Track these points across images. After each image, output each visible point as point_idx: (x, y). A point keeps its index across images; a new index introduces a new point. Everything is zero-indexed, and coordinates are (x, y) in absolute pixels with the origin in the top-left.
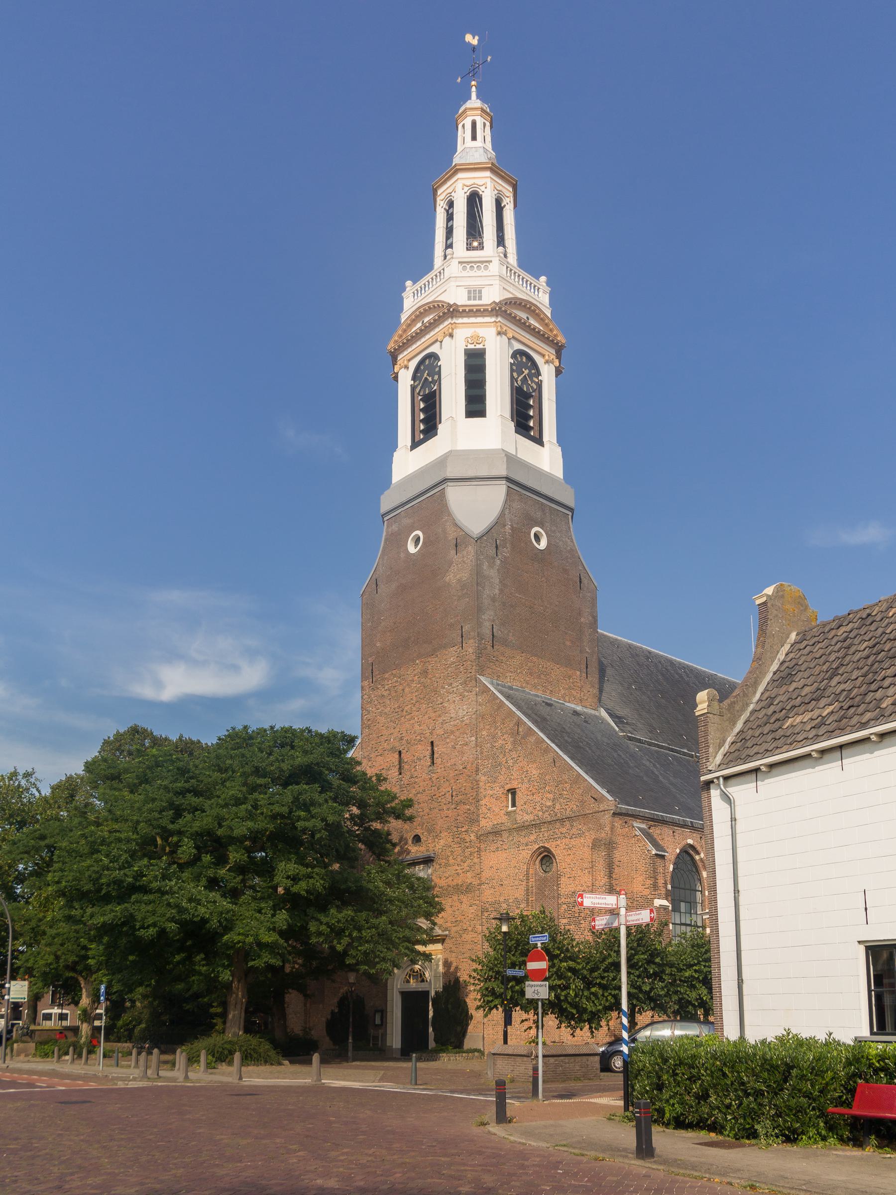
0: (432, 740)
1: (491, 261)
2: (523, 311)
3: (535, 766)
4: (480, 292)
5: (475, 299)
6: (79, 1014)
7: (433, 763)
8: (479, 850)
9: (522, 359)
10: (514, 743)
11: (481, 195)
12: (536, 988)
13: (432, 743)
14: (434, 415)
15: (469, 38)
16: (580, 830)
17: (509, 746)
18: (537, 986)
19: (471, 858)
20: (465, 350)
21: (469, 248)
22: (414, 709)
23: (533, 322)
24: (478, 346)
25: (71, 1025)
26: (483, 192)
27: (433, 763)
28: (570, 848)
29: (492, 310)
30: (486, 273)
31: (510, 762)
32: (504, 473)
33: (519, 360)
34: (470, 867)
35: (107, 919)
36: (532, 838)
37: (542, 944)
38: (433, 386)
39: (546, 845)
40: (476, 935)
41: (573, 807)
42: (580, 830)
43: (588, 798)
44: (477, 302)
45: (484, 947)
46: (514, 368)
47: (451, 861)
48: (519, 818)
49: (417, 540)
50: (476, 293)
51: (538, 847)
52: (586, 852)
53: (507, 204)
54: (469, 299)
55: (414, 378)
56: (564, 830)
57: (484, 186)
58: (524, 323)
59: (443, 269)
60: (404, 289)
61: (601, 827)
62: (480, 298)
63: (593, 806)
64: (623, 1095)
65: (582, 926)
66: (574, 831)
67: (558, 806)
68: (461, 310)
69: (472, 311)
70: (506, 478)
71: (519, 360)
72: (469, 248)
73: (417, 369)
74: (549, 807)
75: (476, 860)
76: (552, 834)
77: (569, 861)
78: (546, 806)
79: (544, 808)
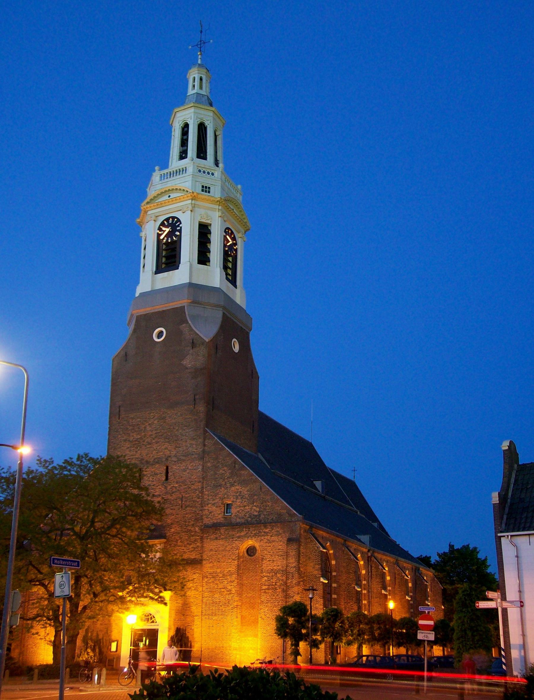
7: (167, 479)
8: (202, 539)
11: (207, 126)
12: (426, 634)
17: (228, 474)
18: (428, 633)
20: (199, 222)
21: (199, 157)
27: (167, 479)
32: (222, 303)
37: (72, 592)
45: (203, 601)
47: (179, 544)
49: (160, 335)
60: (154, 171)
62: (209, 192)
65: (277, 591)
67: (262, 516)
74: (256, 516)
76: (258, 532)
78: (254, 515)
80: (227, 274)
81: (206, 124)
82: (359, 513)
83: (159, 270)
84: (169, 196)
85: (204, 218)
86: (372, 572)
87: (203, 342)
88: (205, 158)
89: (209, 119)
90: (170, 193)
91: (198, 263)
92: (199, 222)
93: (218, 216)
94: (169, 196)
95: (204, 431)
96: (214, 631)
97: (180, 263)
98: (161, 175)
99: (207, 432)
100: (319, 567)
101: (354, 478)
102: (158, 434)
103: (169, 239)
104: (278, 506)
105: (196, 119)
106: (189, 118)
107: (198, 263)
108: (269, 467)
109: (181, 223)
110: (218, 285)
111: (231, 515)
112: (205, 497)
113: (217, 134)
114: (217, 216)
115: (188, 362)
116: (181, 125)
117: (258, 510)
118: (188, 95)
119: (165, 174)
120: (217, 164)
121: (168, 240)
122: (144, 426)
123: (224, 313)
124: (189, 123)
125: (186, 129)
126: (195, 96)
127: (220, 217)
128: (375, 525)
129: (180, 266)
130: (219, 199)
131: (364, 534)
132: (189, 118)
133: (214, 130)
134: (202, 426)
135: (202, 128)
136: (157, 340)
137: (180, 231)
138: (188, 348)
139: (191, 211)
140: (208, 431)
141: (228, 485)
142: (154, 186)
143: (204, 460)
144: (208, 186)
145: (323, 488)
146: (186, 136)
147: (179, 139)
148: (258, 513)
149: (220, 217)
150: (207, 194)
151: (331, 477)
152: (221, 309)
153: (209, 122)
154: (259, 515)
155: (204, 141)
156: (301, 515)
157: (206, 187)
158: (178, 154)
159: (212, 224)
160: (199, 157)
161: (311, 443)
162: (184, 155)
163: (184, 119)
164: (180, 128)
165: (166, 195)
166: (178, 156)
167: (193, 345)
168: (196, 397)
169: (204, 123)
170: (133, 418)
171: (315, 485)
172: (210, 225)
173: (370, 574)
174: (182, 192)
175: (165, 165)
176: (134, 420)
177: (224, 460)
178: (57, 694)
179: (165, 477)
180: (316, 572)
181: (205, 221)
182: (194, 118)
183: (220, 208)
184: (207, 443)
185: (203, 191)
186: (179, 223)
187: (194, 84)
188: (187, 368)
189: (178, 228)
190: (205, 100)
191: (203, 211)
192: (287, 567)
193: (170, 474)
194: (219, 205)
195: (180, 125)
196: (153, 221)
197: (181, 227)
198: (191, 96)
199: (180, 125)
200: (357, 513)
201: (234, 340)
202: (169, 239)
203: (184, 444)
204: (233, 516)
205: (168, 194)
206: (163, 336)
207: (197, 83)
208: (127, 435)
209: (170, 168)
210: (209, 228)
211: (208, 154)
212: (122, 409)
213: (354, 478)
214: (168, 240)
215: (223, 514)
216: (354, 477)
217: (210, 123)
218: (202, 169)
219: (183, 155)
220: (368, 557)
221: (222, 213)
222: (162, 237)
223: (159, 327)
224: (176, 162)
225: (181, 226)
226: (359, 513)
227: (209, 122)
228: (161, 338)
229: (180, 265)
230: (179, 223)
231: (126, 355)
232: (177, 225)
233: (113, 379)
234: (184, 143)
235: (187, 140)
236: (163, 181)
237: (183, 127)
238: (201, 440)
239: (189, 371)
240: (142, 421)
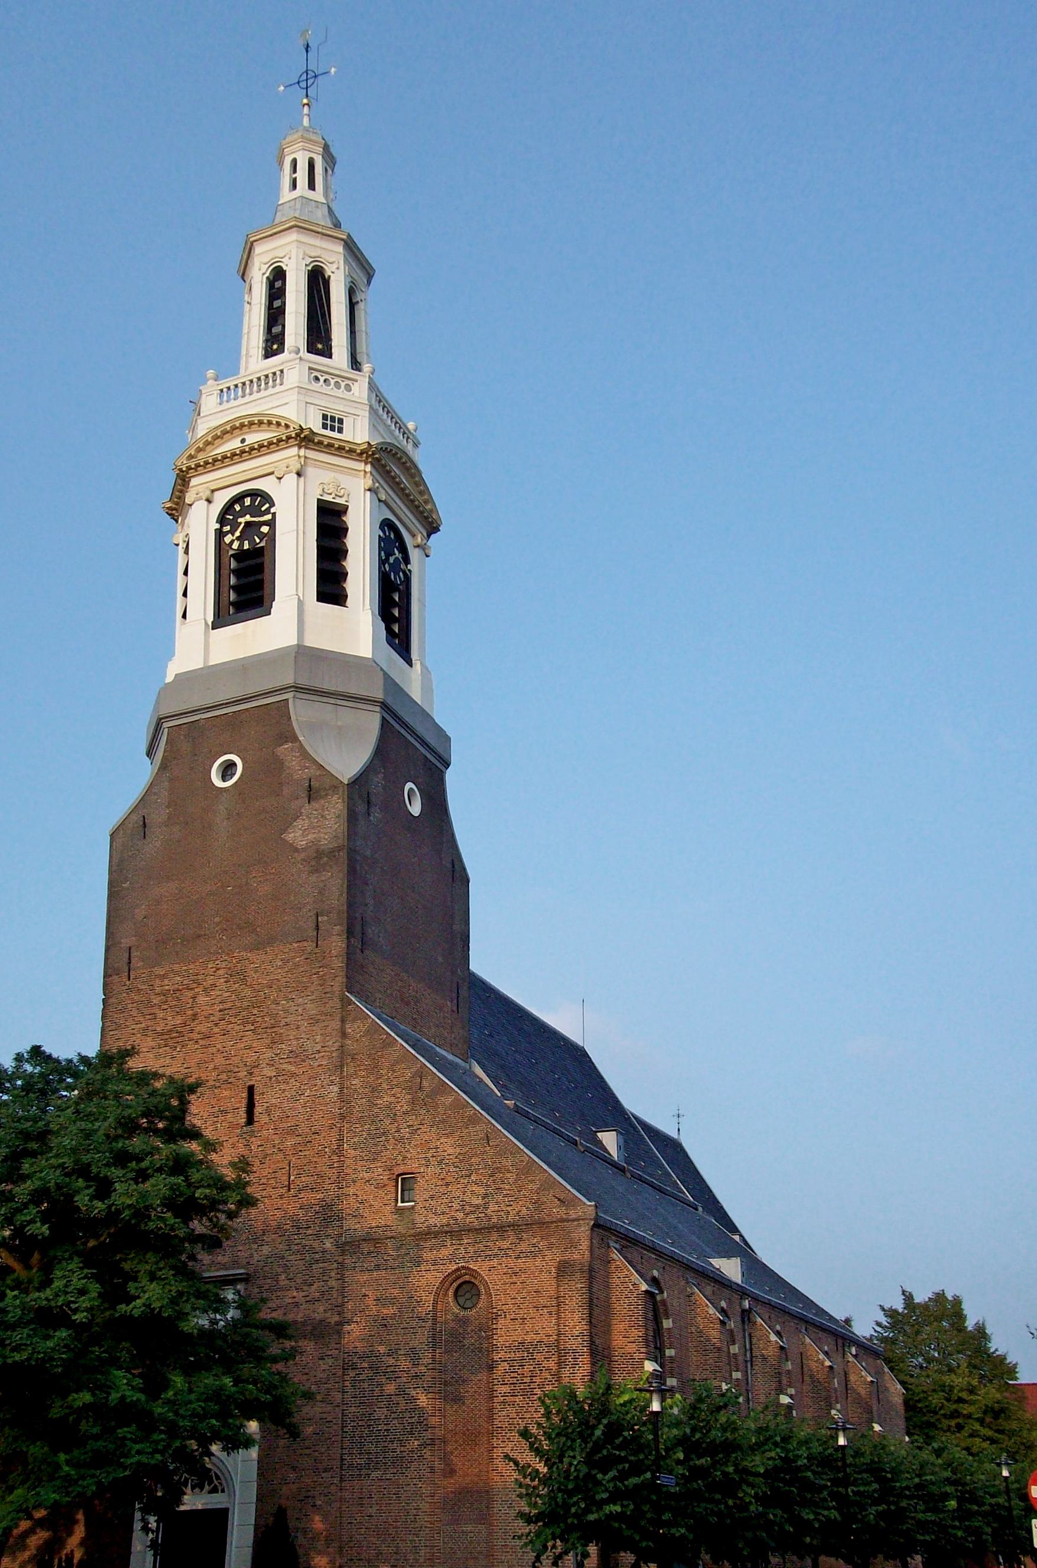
0: (251, 1083)
1: (357, 381)
3: (450, 1141)
4: (341, 421)
5: (333, 429)
7: (250, 1120)
10: (413, 1102)
11: (329, 277)
13: (251, 1090)
14: (260, 585)
15: (192, 1359)
16: (534, 1246)
19: (325, 1278)
21: (312, 349)
22: (216, 1030)
23: (253, 438)
24: (338, 500)
26: (333, 272)
27: (250, 1120)
28: (516, 1274)
29: (361, 454)
30: (347, 395)
31: (405, 1132)
32: (379, 695)
33: (387, 534)
34: (323, 1293)
36: (445, 1252)
38: (258, 540)
39: (471, 1266)
40: (329, 1408)
41: (519, 1210)
42: (534, 1246)
43: (548, 1198)
44: (335, 435)
45: (345, 1430)
48: (420, 1219)
49: (228, 769)
50: (332, 422)
51: (455, 1267)
52: (547, 1282)
53: (361, 300)
54: (325, 426)
55: (222, 520)
56: (505, 1244)
57: (287, 258)
59: (282, 371)
60: (205, 381)
61: (573, 1245)
62: (340, 431)
63: (558, 1211)
66: (523, 1246)
67: (493, 1207)
68: (316, 441)
69: (343, 448)
70: (382, 703)
71: (387, 534)
73: (228, 508)
74: (477, 1206)
75: (333, 1283)
77: (513, 1294)
78: (471, 1205)
79: (467, 1207)
80: (389, 630)
81: (328, 273)
82: (700, 1209)
83: (220, 620)
84: (243, 441)
85: (329, 492)
86: (751, 1349)
87: (335, 785)
88: (327, 353)
89: (334, 260)
91: (318, 600)
92: (319, 500)
93: (365, 490)
94: (243, 441)
95: (342, 1000)
96: (373, 1511)
97: (274, 600)
98: (222, 391)
99: (350, 1002)
100: (640, 1334)
101: (679, 1134)
102: (226, 1012)
103: (246, 542)
104: (532, 1181)
105: (303, 259)
106: (285, 256)
107: (318, 600)
108: (499, 1095)
109: (272, 504)
110: (368, 654)
111: (413, 1207)
112: (348, 1162)
113: (354, 301)
114: (363, 490)
115: (298, 835)
117: (482, 1191)
118: (280, 203)
119: (232, 387)
120: (355, 364)
121: (241, 545)
122: (190, 994)
123: (383, 718)
125: (278, 284)
126: (298, 206)
127: (369, 490)
128: (737, 1238)
129: (273, 605)
130: (365, 446)
131: (729, 1257)
132: (285, 256)
133: (348, 286)
134: (337, 989)
135: (317, 280)
136: (218, 783)
137: (271, 524)
138: (298, 802)
139: (299, 474)
140: (353, 999)
141: (405, 1132)
142: (203, 417)
143: (342, 1072)
145: (619, 1148)
146: (280, 301)
147: (262, 328)
148: (484, 1198)
149: (369, 490)
150: (335, 435)
151: (635, 1128)
152: (378, 709)
153: (335, 266)
154: (486, 1206)
155: (323, 315)
156: (590, 1202)
157: (333, 419)
158: (261, 344)
159: (350, 508)
160: (312, 349)
161: (583, 1047)
162: (275, 347)
163: (272, 259)
164: (265, 280)
165: (238, 436)
166: (260, 349)
167: (312, 793)
168: (320, 919)
169: (322, 267)
170: (163, 977)
171: (601, 1142)
173: (748, 1355)
174: (264, 427)
175: (229, 363)
176: (166, 982)
177: (394, 1071)
179: (245, 1115)
180: (632, 1348)
181: (334, 498)
182: (297, 255)
183: (369, 468)
184: (350, 1031)
186: (267, 505)
187: (294, 176)
188: (296, 850)
190: (323, 215)
192: (558, 1335)
193: (258, 1109)
194: (366, 464)
195: (263, 274)
196: (206, 503)
197: (274, 514)
198: (287, 204)
199: (263, 274)
200: (697, 1209)
201: (409, 785)
202: (246, 542)
203: (293, 1034)
204: (417, 1208)
205: (242, 434)
206: (235, 774)
207: (302, 176)
208: (148, 1017)
209: (242, 372)
211: (334, 343)
212: (134, 954)
213: (679, 1134)
214: (241, 545)
215: (393, 1204)
216: (679, 1130)
217: (338, 268)
218: (322, 376)
219: (274, 343)
220: (743, 1311)
221: (374, 480)
222: (228, 539)
223: (225, 754)
224: (257, 362)
225: (273, 510)
226: (700, 1209)
227: (335, 266)
228: (231, 778)
229: (274, 603)
230: (267, 505)
231: (144, 823)
232: (263, 509)
233: (111, 884)
234: (275, 316)
235: (281, 311)
236: (225, 406)
238: (336, 1024)
239: (303, 855)
240: (185, 982)
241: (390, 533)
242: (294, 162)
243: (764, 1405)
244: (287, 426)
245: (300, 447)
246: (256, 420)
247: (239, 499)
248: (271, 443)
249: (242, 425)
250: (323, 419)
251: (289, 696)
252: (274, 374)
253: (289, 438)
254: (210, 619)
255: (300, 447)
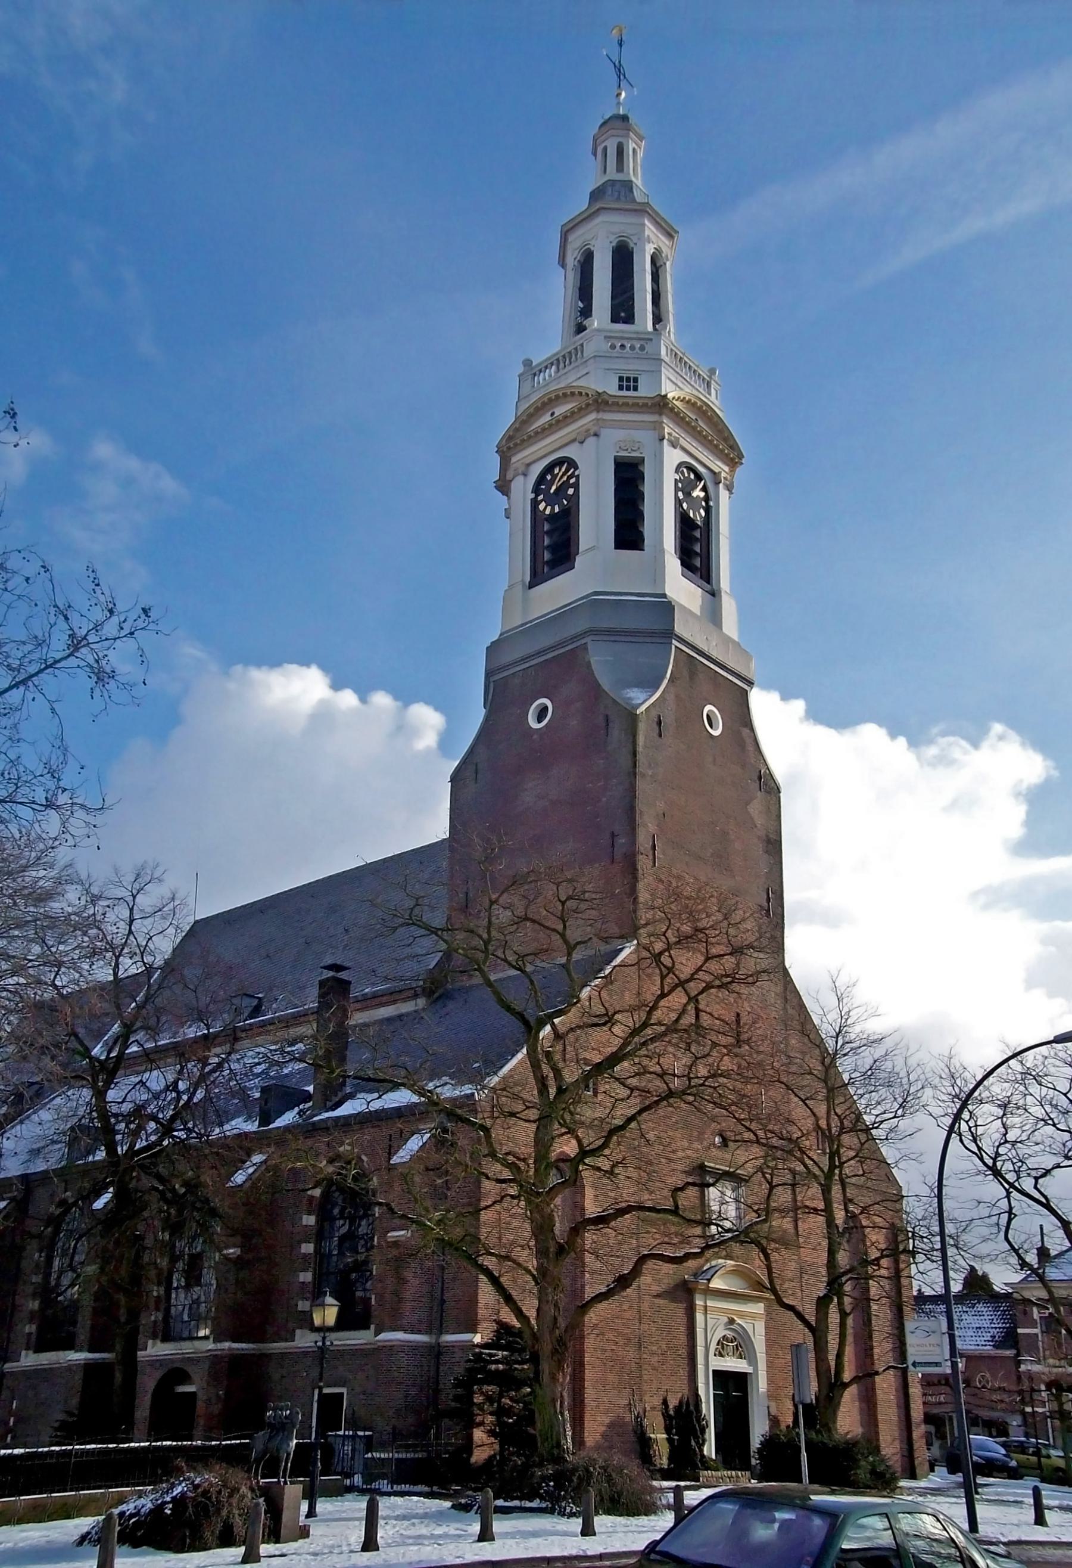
2: (541, 416)
4: (636, 380)
5: (628, 389)
6: (30, 1334)
9: (689, 474)
11: (633, 248)
20: (616, 458)
21: (615, 319)
23: (560, 410)
24: (633, 454)
25: (663, 1431)
26: (636, 244)
33: (686, 475)
35: (527, 1252)
46: (680, 485)
49: (542, 713)
54: (621, 388)
55: (536, 490)
58: (688, 423)
59: (582, 345)
62: (636, 389)
64: (139, 1377)
69: (617, 404)
71: (686, 475)
72: (615, 319)
73: (541, 479)
90: (553, 408)
94: (552, 414)
103: (549, 508)
109: (576, 468)
116: (578, 258)
124: (592, 249)
136: (534, 725)
137: (576, 486)
144: (625, 375)
150: (631, 393)
157: (628, 379)
172: (643, 459)
174: (569, 399)
178: (360, 1510)
185: (622, 390)
186: (572, 470)
189: (572, 481)
191: (620, 434)
202: (549, 508)
205: (549, 410)
210: (641, 469)
230: (572, 470)
237: (582, 261)
241: (689, 474)
242: (605, 149)
243: (437, 1101)
244: (587, 395)
245: (598, 412)
246: (577, 391)
247: (549, 469)
248: (573, 413)
249: (550, 400)
250: (619, 381)
251: (588, 640)
252: (576, 349)
253: (588, 405)
254: (528, 579)
255: (598, 412)
